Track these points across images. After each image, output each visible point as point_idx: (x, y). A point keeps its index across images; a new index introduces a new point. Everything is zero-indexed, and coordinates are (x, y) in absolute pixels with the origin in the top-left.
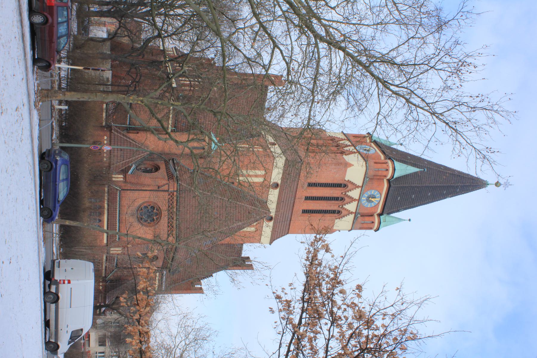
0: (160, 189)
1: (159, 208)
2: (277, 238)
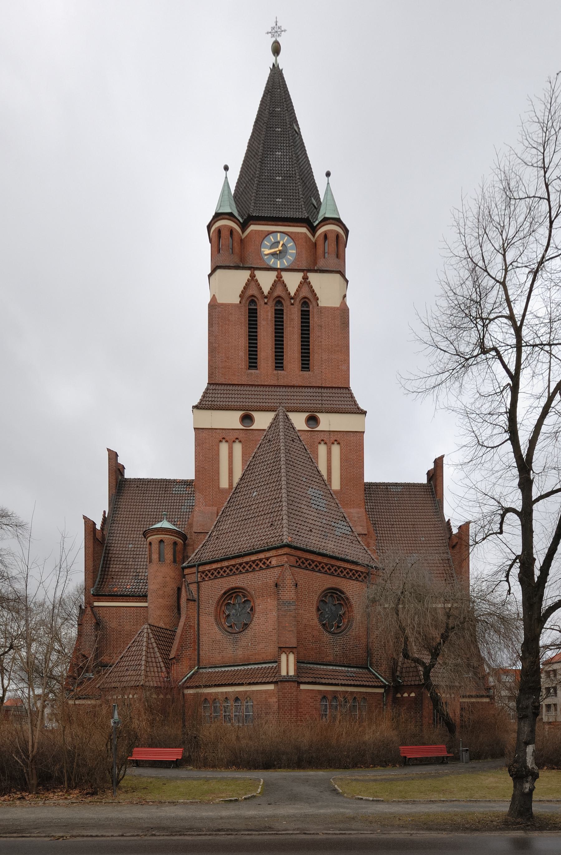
0: (196, 596)
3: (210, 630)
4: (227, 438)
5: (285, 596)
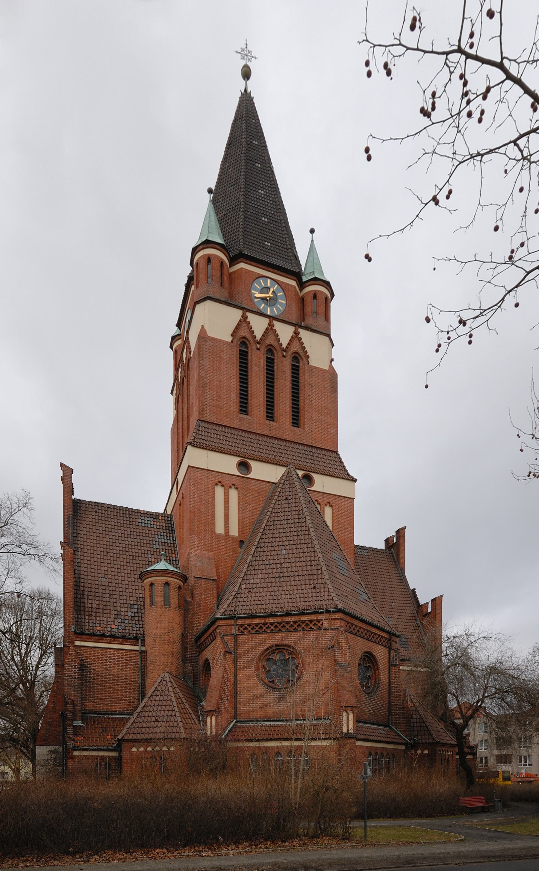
0: (232, 649)
1: (267, 649)
2: (346, 470)
3: (250, 683)
4: (224, 483)
5: (341, 658)
